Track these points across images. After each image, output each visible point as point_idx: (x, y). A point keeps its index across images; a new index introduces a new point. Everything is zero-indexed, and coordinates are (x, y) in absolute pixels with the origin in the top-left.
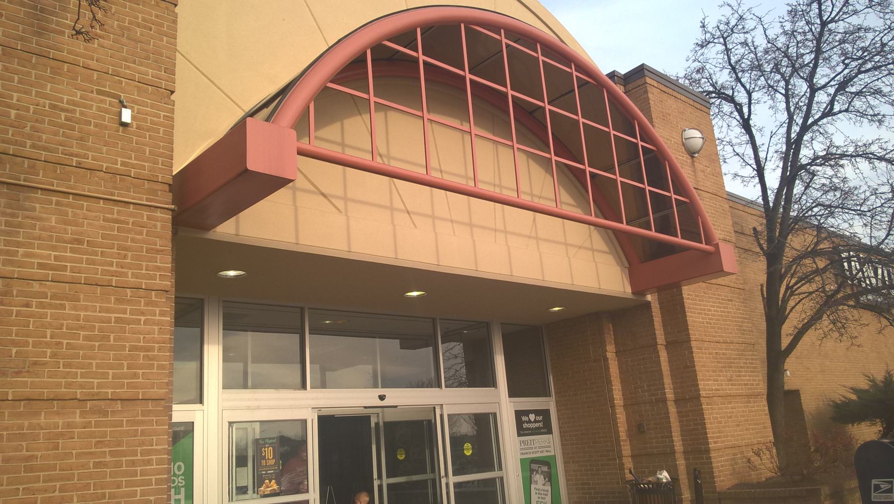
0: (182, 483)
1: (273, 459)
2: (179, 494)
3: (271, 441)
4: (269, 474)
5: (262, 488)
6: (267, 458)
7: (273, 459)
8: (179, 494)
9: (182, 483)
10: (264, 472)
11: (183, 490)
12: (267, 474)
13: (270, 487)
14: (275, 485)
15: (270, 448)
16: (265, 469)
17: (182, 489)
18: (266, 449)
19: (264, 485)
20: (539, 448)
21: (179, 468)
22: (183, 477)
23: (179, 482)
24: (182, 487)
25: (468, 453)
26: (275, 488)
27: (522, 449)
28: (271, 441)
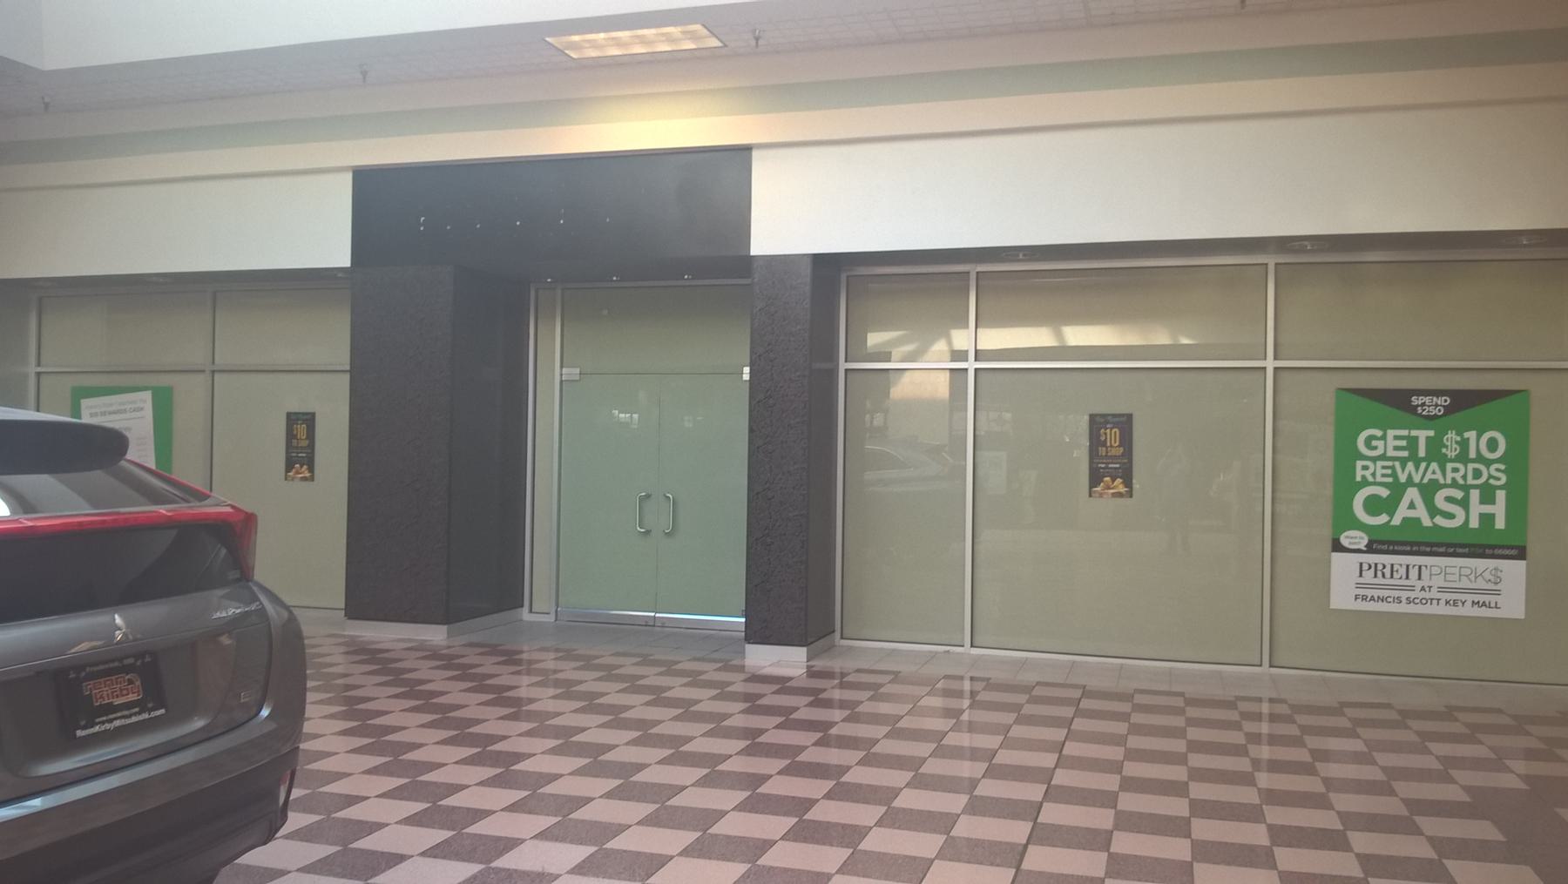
0: (1499, 479)
1: (1119, 446)
2: (1492, 501)
3: (1117, 419)
4: (1111, 468)
5: (1098, 489)
6: (1108, 444)
7: (1119, 446)
8: (1492, 501)
9: (1499, 479)
10: (1103, 466)
11: (1501, 495)
12: (297, 457)
13: (1113, 488)
14: (1121, 486)
15: (1113, 431)
16: (1105, 461)
17: (1498, 492)
18: (1108, 431)
19: (1102, 484)
20: (1442, 590)
21: (1493, 445)
22: (1502, 467)
23: (1490, 476)
24: (1500, 488)
25: (1068, 440)
26: (1121, 490)
27: (1359, 586)
28: (1117, 419)
